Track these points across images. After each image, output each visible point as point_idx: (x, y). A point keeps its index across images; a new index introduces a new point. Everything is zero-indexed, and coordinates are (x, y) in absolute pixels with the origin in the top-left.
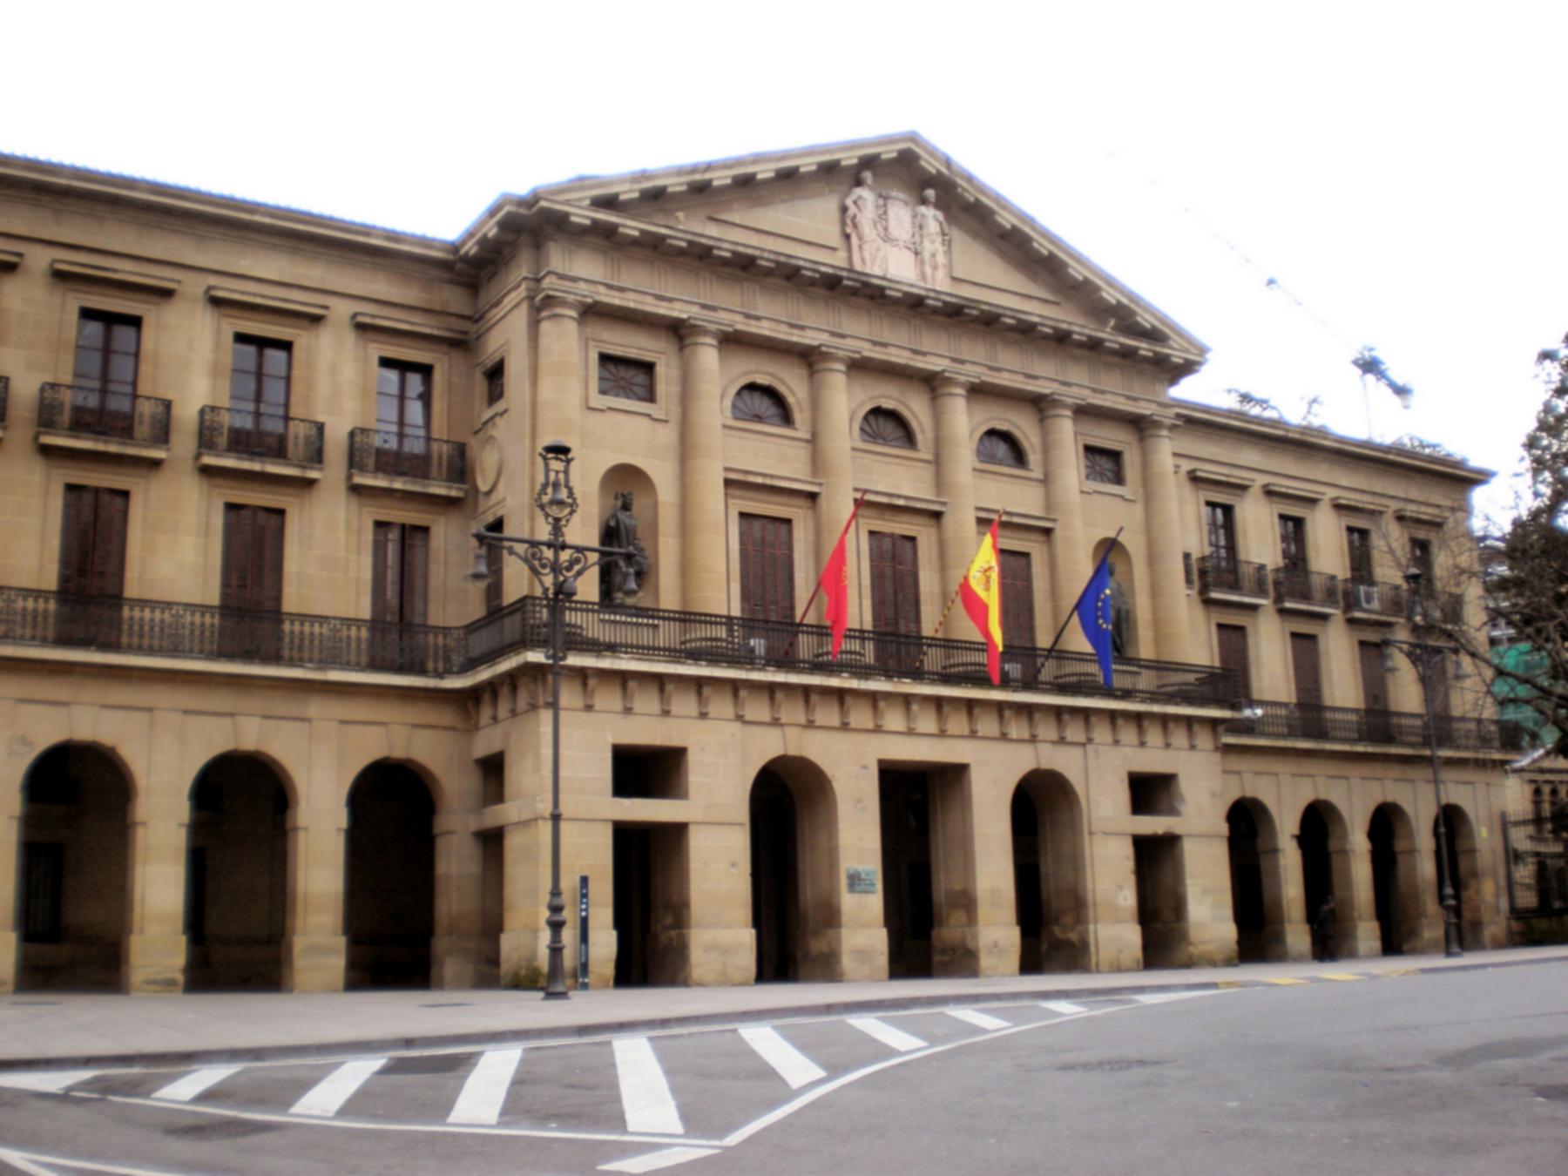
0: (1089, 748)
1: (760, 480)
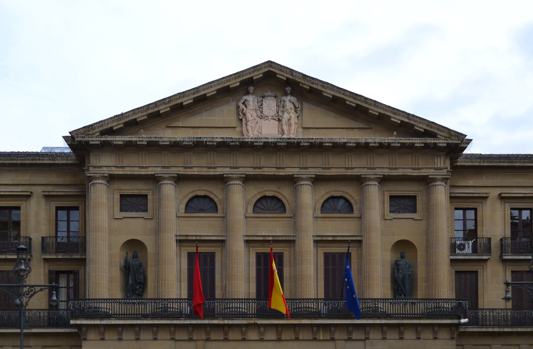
0: (367, 341)
1: (194, 238)
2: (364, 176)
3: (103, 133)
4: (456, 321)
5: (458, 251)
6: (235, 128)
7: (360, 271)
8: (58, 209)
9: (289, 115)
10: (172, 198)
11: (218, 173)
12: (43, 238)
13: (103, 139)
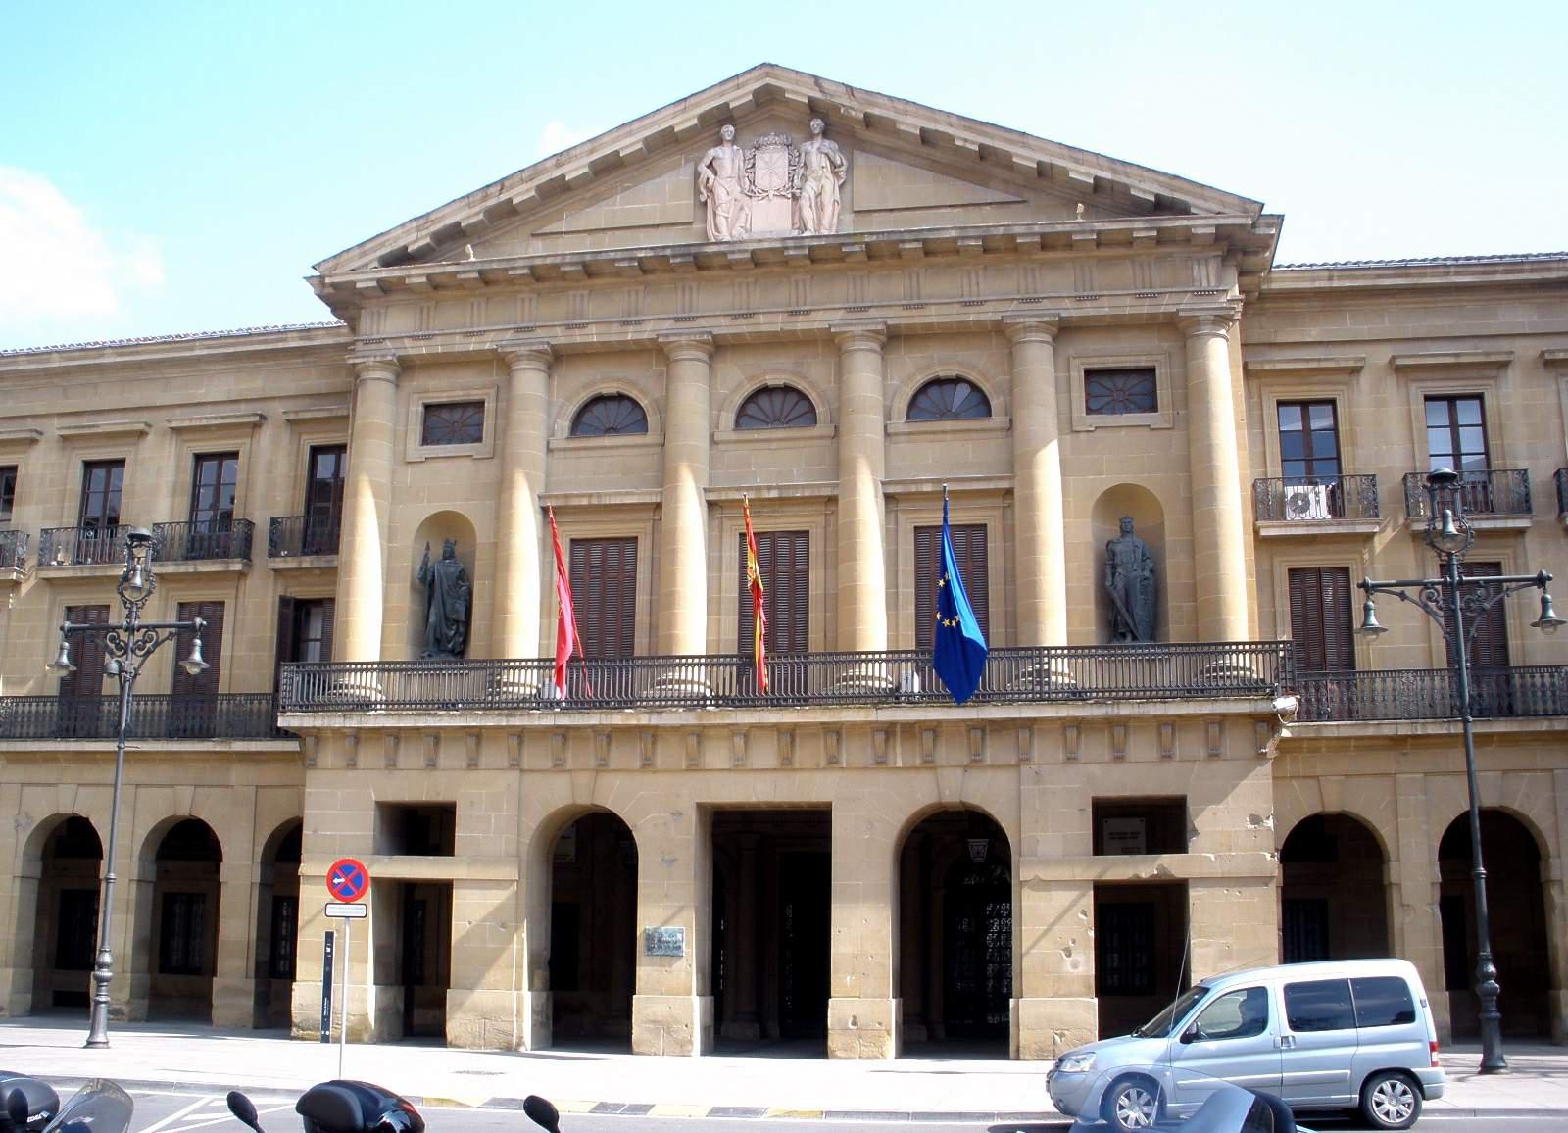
0: (1025, 769)
2: (1009, 321)
3: (389, 261)
4: (1262, 706)
5: (1290, 515)
6: (690, 223)
9: (821, 183)
11: (816, 326)
12: (274, 521)
13: (383, 275)
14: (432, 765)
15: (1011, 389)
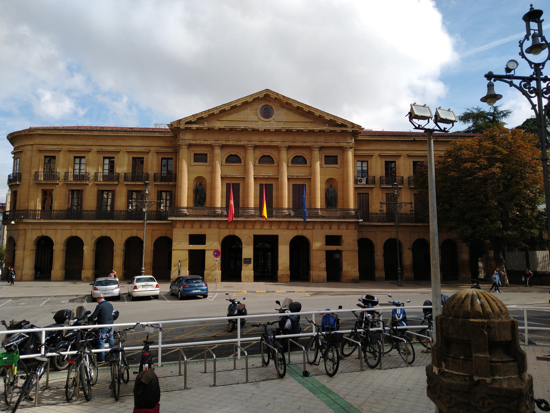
3: (186, 123)
4: (357, 220)
5: (359, 183)
7: (310, 194)
8: (162, 159)
10: (219, 156)
14: (201, 227)
15: (311, 158)
